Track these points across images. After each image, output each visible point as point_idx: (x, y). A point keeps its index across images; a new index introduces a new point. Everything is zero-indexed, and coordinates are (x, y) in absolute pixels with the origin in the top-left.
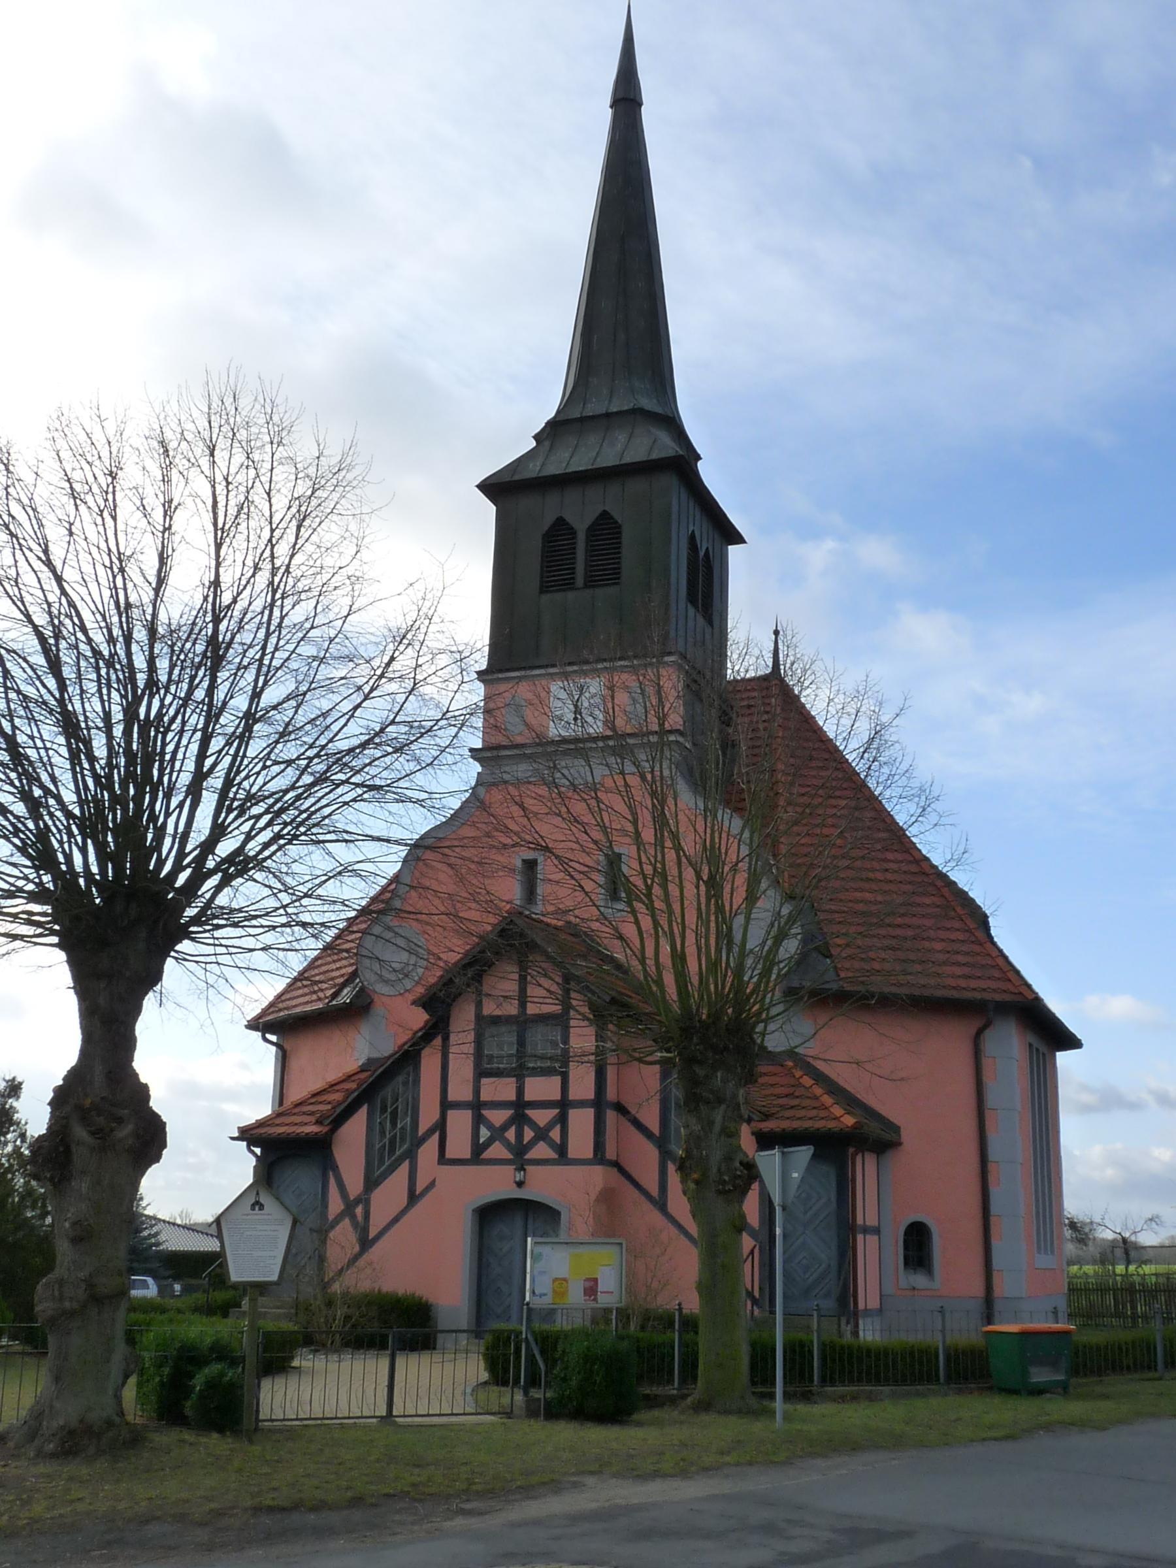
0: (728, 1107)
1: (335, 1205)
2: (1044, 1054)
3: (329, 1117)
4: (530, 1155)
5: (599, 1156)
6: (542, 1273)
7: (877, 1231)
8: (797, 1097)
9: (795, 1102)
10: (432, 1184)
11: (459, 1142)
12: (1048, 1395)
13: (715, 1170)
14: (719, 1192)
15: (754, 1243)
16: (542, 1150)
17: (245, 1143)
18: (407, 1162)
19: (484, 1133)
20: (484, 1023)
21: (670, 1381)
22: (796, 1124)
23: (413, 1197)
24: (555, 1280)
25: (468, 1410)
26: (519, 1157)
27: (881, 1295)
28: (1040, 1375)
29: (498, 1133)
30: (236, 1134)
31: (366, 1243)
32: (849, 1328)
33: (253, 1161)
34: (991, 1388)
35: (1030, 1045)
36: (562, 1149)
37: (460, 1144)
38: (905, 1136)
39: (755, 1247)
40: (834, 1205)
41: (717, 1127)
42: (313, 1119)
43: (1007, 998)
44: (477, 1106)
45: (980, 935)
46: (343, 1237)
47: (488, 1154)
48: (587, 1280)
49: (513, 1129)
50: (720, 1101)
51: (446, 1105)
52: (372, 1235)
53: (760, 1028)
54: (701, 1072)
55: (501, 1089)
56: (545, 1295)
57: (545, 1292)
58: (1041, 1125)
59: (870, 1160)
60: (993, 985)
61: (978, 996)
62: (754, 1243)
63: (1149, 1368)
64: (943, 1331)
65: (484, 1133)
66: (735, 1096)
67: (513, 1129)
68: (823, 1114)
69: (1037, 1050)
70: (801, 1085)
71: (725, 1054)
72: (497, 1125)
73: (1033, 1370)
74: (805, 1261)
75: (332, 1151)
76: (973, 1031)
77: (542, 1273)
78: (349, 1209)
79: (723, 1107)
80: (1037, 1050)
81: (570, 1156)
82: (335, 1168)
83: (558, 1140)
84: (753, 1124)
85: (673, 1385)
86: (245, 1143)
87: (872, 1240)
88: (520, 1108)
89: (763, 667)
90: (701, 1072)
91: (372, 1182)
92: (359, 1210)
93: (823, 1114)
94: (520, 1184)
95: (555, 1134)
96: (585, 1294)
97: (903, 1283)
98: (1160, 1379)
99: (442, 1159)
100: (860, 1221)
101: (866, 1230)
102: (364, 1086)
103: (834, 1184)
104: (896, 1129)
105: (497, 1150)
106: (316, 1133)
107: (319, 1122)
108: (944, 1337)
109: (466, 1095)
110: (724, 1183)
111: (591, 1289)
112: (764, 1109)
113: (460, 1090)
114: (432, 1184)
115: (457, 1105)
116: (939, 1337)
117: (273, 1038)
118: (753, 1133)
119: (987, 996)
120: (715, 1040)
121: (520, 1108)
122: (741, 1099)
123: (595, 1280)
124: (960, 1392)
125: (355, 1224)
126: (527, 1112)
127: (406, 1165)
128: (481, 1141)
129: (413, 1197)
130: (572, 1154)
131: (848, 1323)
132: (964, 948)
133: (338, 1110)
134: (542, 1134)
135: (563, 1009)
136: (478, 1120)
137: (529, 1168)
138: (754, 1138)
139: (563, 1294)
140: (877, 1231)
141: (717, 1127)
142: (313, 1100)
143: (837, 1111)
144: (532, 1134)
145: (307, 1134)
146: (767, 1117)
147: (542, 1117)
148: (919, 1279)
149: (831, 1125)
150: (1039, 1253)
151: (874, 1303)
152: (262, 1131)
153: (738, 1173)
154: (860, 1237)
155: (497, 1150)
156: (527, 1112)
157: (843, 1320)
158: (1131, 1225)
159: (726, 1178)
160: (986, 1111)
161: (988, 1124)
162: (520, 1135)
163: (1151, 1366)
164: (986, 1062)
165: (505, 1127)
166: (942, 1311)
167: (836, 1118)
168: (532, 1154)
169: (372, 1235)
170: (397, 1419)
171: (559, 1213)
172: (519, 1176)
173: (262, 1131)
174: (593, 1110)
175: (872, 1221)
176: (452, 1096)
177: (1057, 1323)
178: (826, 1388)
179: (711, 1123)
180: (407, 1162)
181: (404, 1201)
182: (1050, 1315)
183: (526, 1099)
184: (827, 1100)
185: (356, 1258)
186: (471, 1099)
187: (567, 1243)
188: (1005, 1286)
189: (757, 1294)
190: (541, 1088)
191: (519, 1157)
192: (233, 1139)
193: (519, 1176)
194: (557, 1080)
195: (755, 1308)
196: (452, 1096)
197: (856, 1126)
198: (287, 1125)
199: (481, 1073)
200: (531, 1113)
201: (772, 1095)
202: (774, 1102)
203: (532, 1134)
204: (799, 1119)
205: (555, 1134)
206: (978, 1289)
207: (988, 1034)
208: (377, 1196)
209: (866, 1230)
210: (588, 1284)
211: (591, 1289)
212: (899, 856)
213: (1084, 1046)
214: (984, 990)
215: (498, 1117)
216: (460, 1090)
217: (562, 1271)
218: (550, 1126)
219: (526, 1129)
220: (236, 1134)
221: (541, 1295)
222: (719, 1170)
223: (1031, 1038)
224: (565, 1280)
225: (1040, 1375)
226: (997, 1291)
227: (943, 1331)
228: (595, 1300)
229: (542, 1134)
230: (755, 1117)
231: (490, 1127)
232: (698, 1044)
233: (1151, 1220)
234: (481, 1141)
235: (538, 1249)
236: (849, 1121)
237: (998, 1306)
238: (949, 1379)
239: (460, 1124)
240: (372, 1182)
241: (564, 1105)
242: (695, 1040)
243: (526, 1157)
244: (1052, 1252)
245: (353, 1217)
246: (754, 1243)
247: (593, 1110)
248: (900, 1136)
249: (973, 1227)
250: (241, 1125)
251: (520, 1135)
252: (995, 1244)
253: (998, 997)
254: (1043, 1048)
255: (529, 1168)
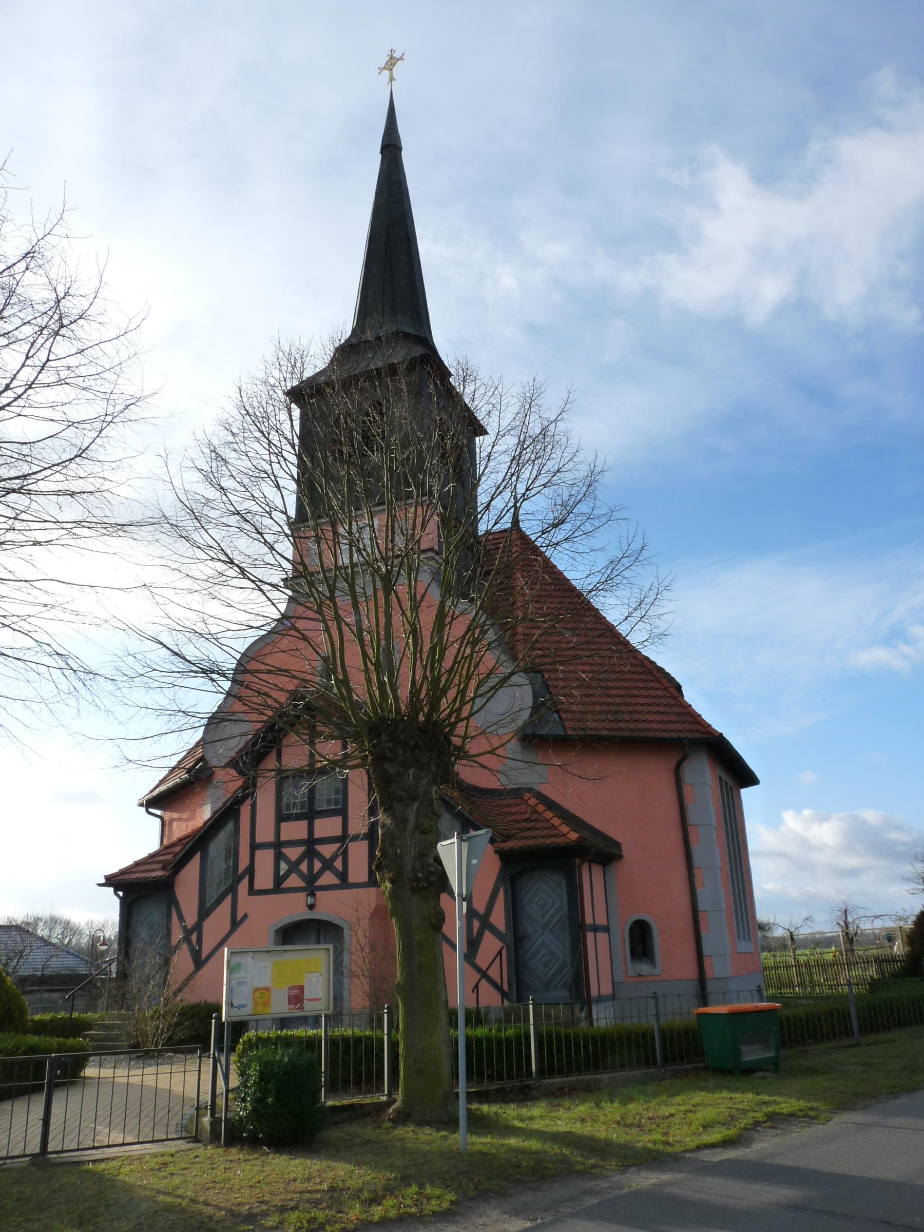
0: (421, 803)
1: (177, 935)
2: (731, 788)
3: (170, 864)
4: (319, 883)
5: (372, 882)
6: (241, 984)
7: (606, 929)
8: (533, 821)
9: (532, 824)
10: (245, 916)
11: (264, 879)
12: (760, 1073)
13: (409, 868)
14: (413, 890)
15: (500, 944)
16: (328, 878)
17: (112, 889)
18: (230, 895)
19: (284, 867)
20: (282, 777)
21: (380, 1089)
22: (531, 842)
23: (235, 924)
24: (256, 990)
25: (129, 1139)
26: (311, 887)
27: (613, 983)
28: (751, 1054)
29: (294, 867)
30: (103, 881)
31: (199, 962)
32: (583, 1014)
33: (117, 901)
34: (705, 1069)
35: (720, 778)
36: (343, 876)
37: (264, 879)
38: (625, 850)
39: (503, 947)
40: (565, 910)
41: (411, 825)
42: (160, 866)
43: (699, 735)
44: (278, 846)
45: (675, 693)
46: (182, 960)
47: (287, 884)
48: (292, 988)
49: (305, 862)
50: (413, 798)
51: (254, 846)
52: (204, 956)
53: (460, 729)
54: (392, 769)
55: (295, 830)
56: (244, 1006)
57: (244, 1002)
58: (734, 850)
59: (597, 871)
60: (686, 726)
61: (675, 735)
62: (502, 945)
63: (847, 1035)
64: (657, 1016)
65: (284, 867)
66: (428, 792)
67: (305, 862)
68: (554, 832)
69: (726, 783)
70: (536, 812)
71: (417, 752)
72: (293, 860)
73: (744, 1049)
74: (544, 958)
75: (174, 891)
76: (674, 765)
77: (241, 984)
78: (188, 932)
79: (417, 804)
80: (726, 783)
81: (350, 881)
82: (177, 904)
83: (340, 868)
84: (496, 844)
85: (384, 1091)
86: (112, 889)
87: (602, 937)
88: (311, 844)
89: (506, 523)
90: (392, 769)
91: (204, 913)
92: (194, 937)
93: (554, 832)
94: (311, 907)
95: (338, 864)
96: (289, 1004)
97: (631, 972)
98: (857, 1045)
99: (252, 891)
100: (589, 920)
101: (596, 929)
102: (198, 836)
103: (565, 891)
104: (618, 845)
105: (294, 881)
106: (161, 877)
107: (163, 868)
108: (658, 1022)
109: (271, 838)
110: (418, 880)
111: (297, 997)
112: (505, 832)
113: (265, 833)
114: (245, 916)
115: (263, 846)
116: (652, 1021)
117: (158, 812)
118: (496, 852)
119: (682, 735)
120: (403, 737)
121: (311, 844)
122: (434, 796)
123: (301, 988)
124: (676, 1074)
125: (190, 943)
126: (316, 847)
127: (228, 900)
128: (282, 873)
129: (235, 924)
130: (352, 879)
131: (582, 1010)
132: (664, 701)
133: (178, 857)
134: (328, 865)
135: (466, 825)
136: (279, 856)
137: (318, 893)
138: (497, 856)
139: (266, 1004)
140: (606, 929)
141: (411, 825)
142: (165, 852)
143: (565, 829)
144: (320, 865)
145: (154, 877)
146: (507, 838)
147: (327, 850)
148: (644, 968)
149: (559, 840)
150: (739, 939)
151: (607, 990)
152: (123, 877)
153: (432, 869)
154: (590, 936)
155: (294, 881)
156: (316, 847)
157: (577, 1007)
158: (794, 924)
159: (420, 875)
160: (689, 827)
161: (692, 838)
162: (311, 866)
163: (848, 1033)
164: (686, 790)
165: (299, 861)
166: (655, 997)
167: (564, 835)
168: (321, 882)
169: (204, 956)
170: (50, 1156)
171: (342, 929)
172: (310, 900)
173: (123, 877)
174: (367, 842)
175: (601, 920)
176: (259, 839)
177: (762, 1002)
178: (546, 1081)
179: (405, 821)
180: (230, 895)
181: (227, 927)
182: (755, 994)
183: (316, 836)
184: (556, 821)
185: (192, 975)
186: (273, 840)
187: (268, 952)
188: (717, 968)
189: (506, 987)
190: (327, 827)
191: (311, 887)
192: (100, 885)
193: (310, 900)
194: (338, 820)
195: (505, 1000)
196: (259, 839)
197: (578, 841)
198: (141, 872)
199: (282, 817)
200: (320, 848)
201: (512, 821)
202: (514, 826)
203: (320, 865)
204: (534, 837)
205: (338, 864)
206: (691, 971)
207: (685, 765)
208: (208, 924)
209: (596, 929)
210: (296, 992)
211: (297, 997)
212: (609, 640)
213: (761, 783)
214: (680, 731)
215: (293, 853)
216: (265, 833)
217: (264, 982)
218: (334, 858)
219: (316, 861)
220: (103, 881)
221: (239, 1007)
222: (414, 866)
223: (720, 772)
224: (267, 989)
225: (751, 1054)
226: (709, 974)
227: (657, 1016)
228: (302, 1008)
229: (328, 865)
230: (498, 839)
231: (288, 861)
232: (386, 741)
233: (807, 919)
234: (315, 871)
235: (236, 959)
236: (574, 836)
237: (711, 987)
238: (666, 1060)
239: (265, 859)
240: (204, 913)
241: (343, 838)
242: (384, 738)
243: (316, 884)
244: (750, 940)
245: (190, 943)
246: (502, 945)
247: (367, 842)
248: (620, 850)
249: (685, 922)
250: (107, 874)
251: (311, 866)
252: (704, 934)
253: (690, 736)
254: (731, 783)
255: (318, 893)
